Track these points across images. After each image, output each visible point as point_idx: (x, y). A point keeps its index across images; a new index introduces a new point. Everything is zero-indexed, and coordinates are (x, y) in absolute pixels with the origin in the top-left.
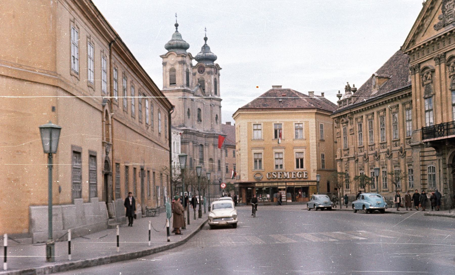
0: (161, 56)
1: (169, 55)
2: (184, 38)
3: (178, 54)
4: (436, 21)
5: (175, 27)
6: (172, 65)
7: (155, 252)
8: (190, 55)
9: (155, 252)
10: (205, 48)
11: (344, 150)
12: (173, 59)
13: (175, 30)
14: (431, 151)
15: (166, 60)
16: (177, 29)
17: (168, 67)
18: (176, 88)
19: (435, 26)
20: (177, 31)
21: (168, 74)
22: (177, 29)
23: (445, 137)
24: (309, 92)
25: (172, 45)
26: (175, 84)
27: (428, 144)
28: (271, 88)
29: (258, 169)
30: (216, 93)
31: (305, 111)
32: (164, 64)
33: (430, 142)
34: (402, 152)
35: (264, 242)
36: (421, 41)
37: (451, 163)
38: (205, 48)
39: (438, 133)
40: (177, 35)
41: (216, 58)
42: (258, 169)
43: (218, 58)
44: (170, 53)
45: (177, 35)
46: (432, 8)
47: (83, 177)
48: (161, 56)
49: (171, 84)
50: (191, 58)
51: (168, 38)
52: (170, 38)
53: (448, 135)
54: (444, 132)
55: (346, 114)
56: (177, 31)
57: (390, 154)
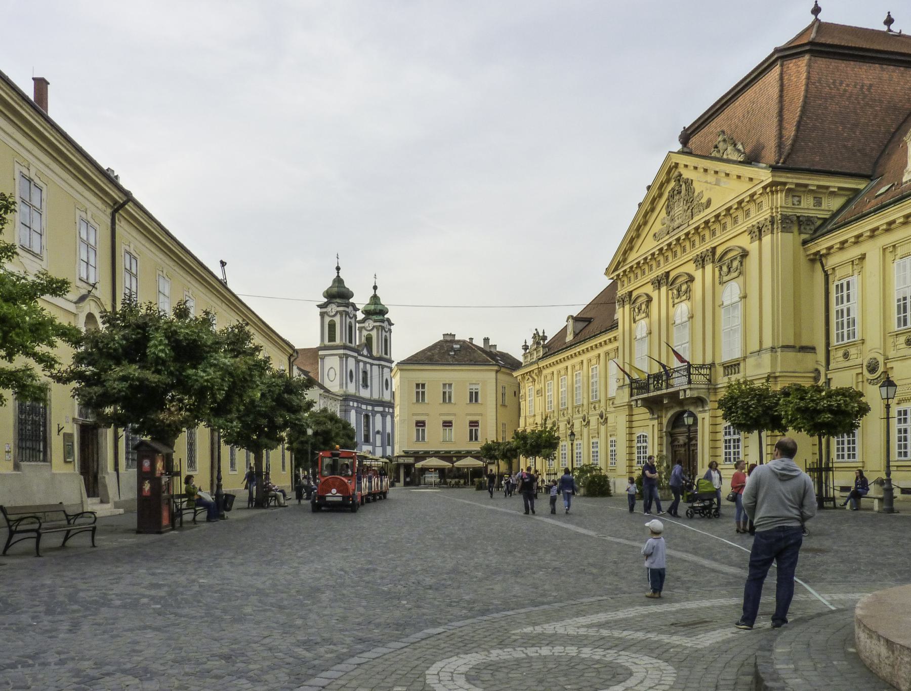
0: (318, 306)
2: (346, 285)
4: (657, 227)
8: (353, 305)
10: (375, 299)
11: (531, 417)
12: (332, 309)
14: (642, 413)
16: (338, 273)
19: (655, 235)
22: (338, 273)
23: (664, 391)
27: (639, 402)
28: (442, 338)
29: (668, 551)
30: (386, 354)
32: (322, 315)
33: (642, 399)
34: (602, 418)
35: (161, 416)
36: (634, 257)
37: (670, 430)
38: (375, 299)
39: (654, 386)
40: (339, 281)
41: (795, 444)
42: (668, 551)
43: (796, 441)
45: (339, 281)
46: (653, 210)
48: (318, 306)
50: (356, 309)
53: (667, 388)
54: (662, 385)
55: (533, 371)
57: (587, 420)
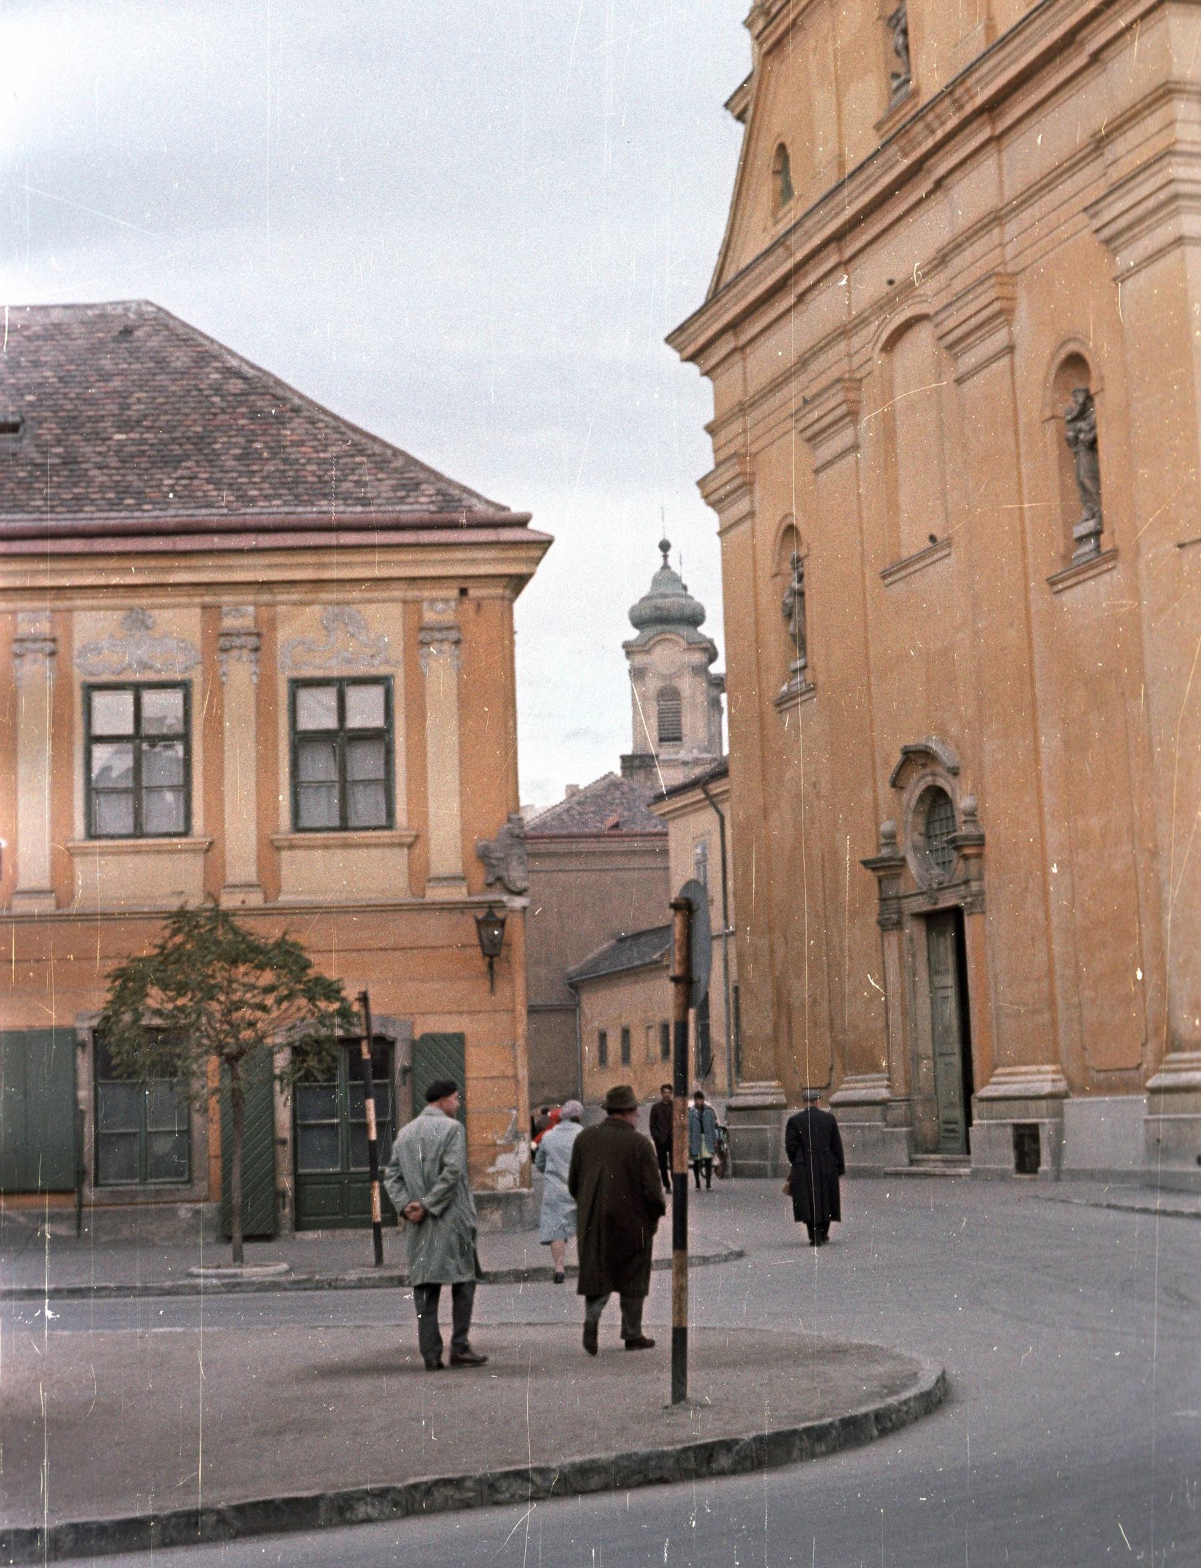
1: (654, 645)
3: (689, 644)
5: (661, 553)
6: (663, 677)
7: (875, 799)
9: (875, 799)
13: (661, 562)
15: (641, 659)
16: (665, 557)
17: (653, 684)
18: (683, 755)
20: (666, 567)
21: (653, 708)
22: (665, 557)
24: (669, 340)
25: (668, 610)
26: (679, 739)
31: (772, 314)
32: (637, 674)
40: (667, 577)
44: (663, 637)
47: (1101, 445)
49: (661, 740)
51: (638, 588)
52: (645, 589)
56: (666, 567)
